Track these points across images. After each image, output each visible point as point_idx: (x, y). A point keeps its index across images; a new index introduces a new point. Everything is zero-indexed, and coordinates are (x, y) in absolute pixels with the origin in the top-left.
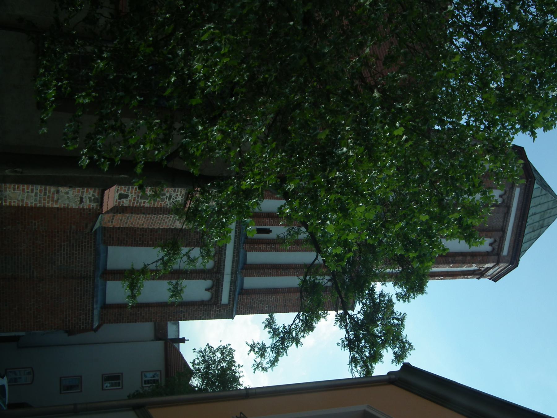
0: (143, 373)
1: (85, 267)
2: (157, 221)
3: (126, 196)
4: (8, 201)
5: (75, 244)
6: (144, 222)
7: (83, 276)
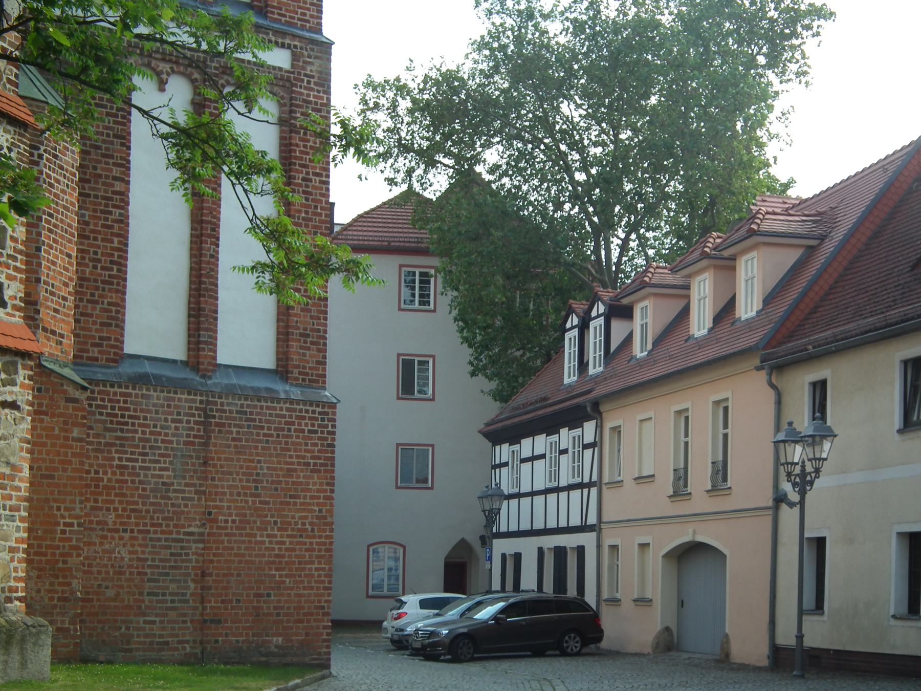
0: (403, 306)
1: (179, 414)
2: (60, 216)
4: (12, 583)
5: (119, 434)
6: (61, 252)
7: (202, 419)
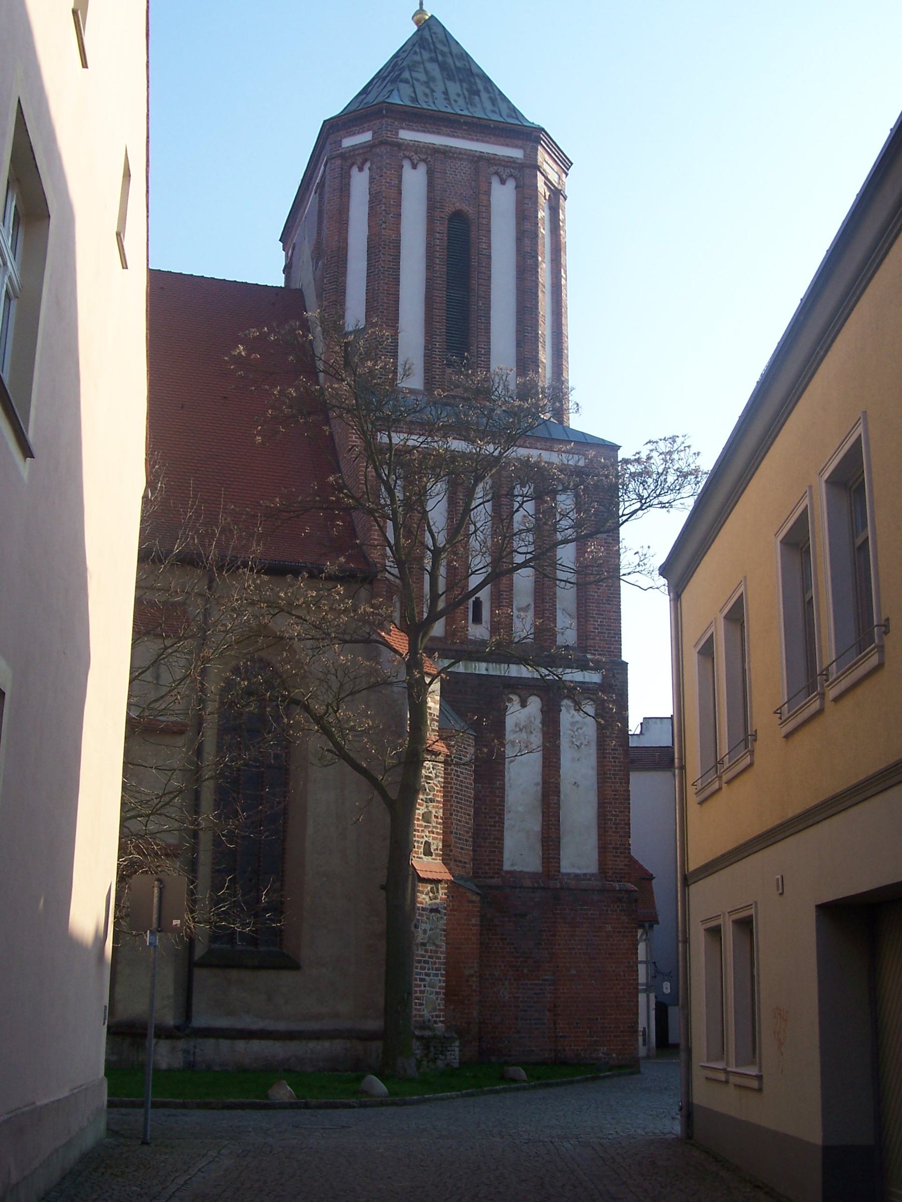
2: (463, 793)
3: (427, 844)
6: (465, 813)
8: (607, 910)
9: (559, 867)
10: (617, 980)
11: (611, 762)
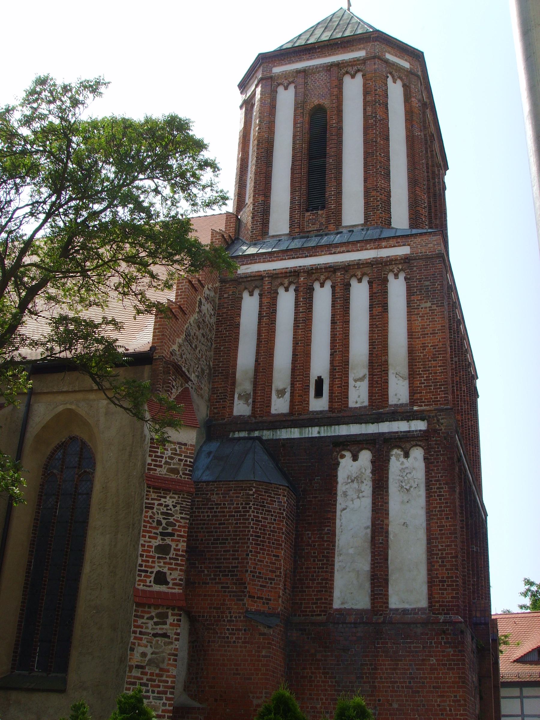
8: (431, 643)
9: (387, 603)
10: (442, 714)
11: (437, 500)
